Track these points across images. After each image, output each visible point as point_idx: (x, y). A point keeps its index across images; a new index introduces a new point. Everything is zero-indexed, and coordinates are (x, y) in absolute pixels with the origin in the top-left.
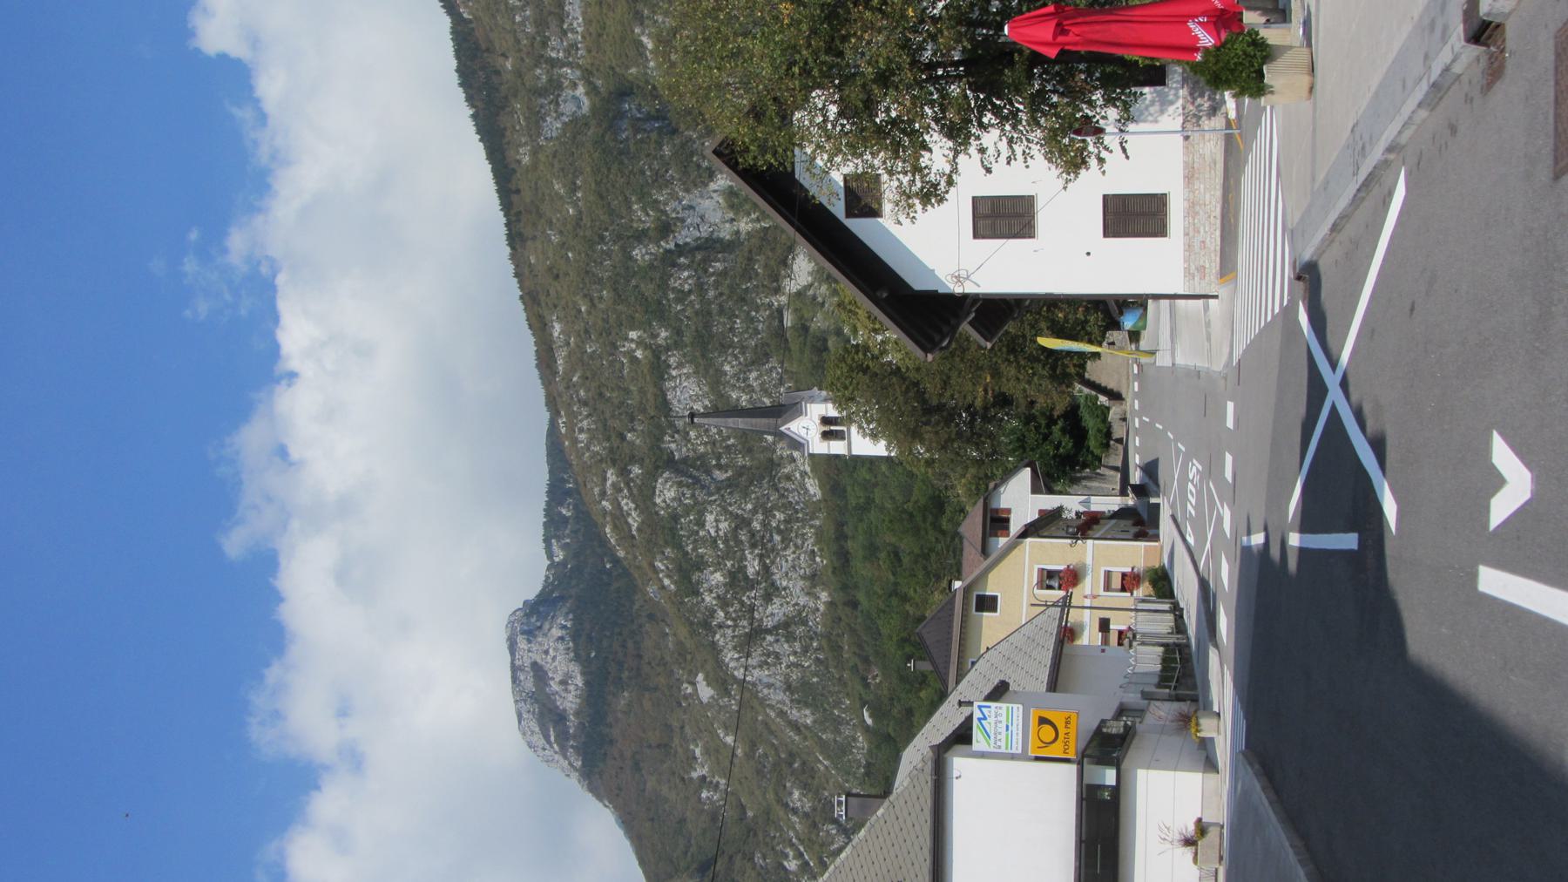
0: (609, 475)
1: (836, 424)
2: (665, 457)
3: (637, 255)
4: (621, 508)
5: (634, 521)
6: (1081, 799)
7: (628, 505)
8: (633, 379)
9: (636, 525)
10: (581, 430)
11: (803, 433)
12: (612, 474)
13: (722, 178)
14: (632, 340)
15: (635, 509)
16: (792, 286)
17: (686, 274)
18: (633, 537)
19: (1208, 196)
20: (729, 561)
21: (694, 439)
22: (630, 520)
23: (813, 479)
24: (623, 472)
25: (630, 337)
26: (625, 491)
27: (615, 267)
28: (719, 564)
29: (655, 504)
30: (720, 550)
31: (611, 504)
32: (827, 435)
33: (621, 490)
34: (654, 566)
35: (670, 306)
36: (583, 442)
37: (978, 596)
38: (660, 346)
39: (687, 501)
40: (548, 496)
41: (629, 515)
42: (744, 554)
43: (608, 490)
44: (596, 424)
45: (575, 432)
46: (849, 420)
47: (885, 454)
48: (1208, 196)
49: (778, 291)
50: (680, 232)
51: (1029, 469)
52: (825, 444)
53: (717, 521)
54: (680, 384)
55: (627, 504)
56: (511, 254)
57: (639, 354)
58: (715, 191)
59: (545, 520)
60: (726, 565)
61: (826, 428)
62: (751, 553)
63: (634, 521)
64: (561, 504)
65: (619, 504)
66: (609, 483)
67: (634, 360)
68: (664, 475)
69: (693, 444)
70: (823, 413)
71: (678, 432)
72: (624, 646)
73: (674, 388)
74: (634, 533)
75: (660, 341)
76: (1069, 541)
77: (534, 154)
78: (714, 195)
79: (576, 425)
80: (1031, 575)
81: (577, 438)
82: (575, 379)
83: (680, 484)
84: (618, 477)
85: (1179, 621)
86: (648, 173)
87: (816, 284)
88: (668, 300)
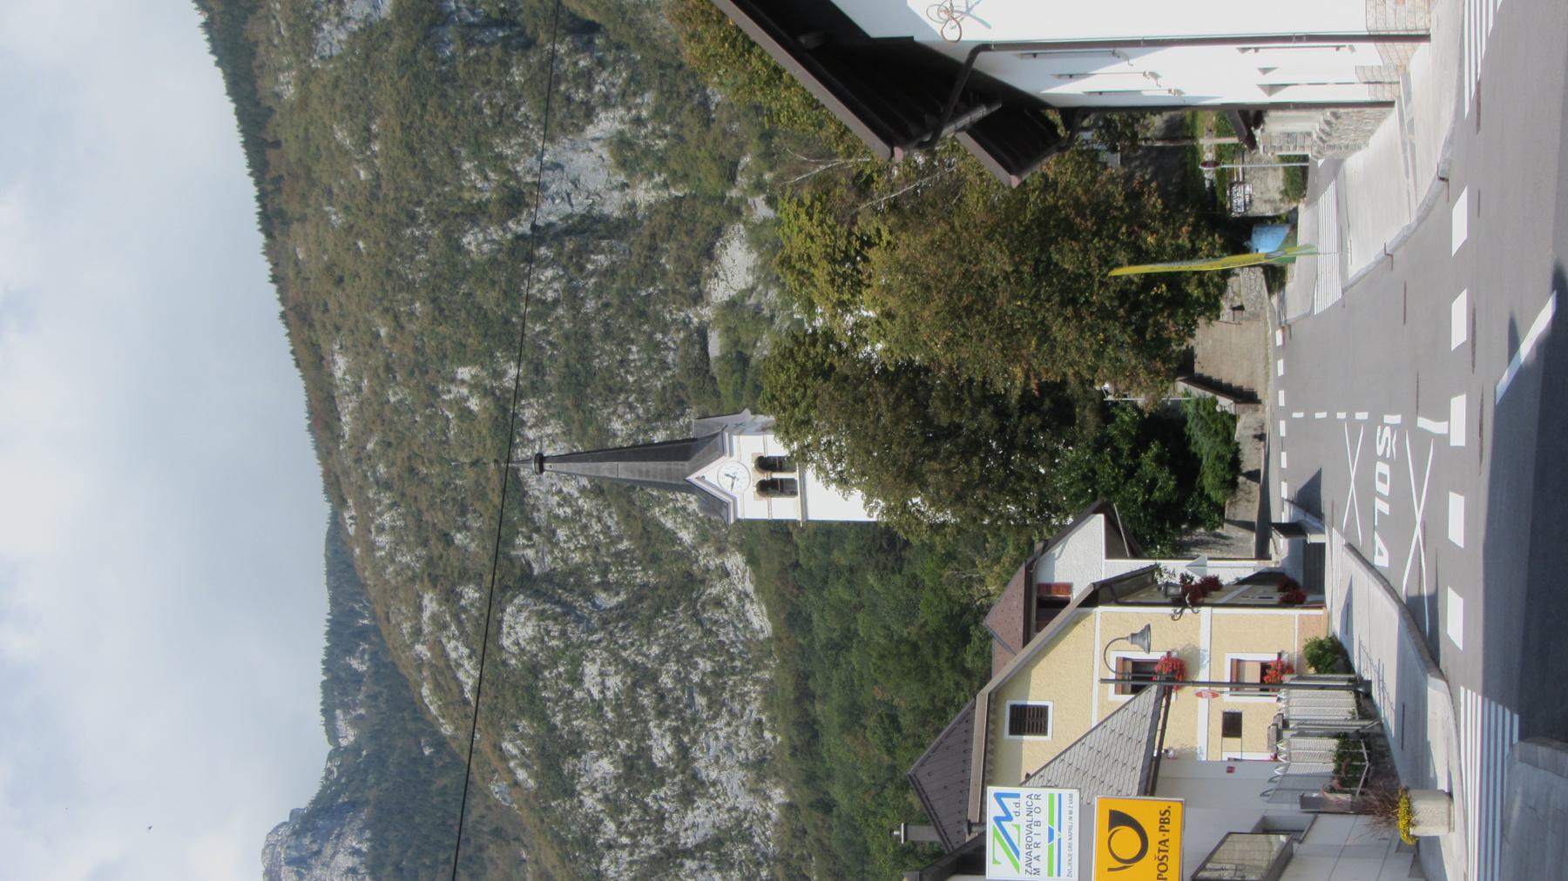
0: (426, 602)
1: (781, 470)
2: (518, 572)
5: (468, 676)
9: (471, 682)
10: (381, 529)
11: (725, 484)
13: (607, 119)
14: (463, 382)
15: (470, 657)
16: (719, 292)
17: (549, 273)
21: (565, 542)
22: (461, 675)
24: (450, 596)
25: (459, 377)
28: (606, 744)
29: (502, 648)
32: (766, 488)
37: (1014, 708)
40: (328, 640)
41: (460, 666)
49: (698, 298)
56: (266, 246)
57: (474, 404)
59: (325, 678)
61: (766, 476)
62: (659, 726)
64: (350, 652)
65: (443, 649)
66: (426, 615)
67: (465, 414)
68: (516, 601)
69: (562, 550)
70: (761, 451)
76: (1170, 610)
78: (594, 146)
83: (542, 615)
84: (440, 605)
87: (760, 287)
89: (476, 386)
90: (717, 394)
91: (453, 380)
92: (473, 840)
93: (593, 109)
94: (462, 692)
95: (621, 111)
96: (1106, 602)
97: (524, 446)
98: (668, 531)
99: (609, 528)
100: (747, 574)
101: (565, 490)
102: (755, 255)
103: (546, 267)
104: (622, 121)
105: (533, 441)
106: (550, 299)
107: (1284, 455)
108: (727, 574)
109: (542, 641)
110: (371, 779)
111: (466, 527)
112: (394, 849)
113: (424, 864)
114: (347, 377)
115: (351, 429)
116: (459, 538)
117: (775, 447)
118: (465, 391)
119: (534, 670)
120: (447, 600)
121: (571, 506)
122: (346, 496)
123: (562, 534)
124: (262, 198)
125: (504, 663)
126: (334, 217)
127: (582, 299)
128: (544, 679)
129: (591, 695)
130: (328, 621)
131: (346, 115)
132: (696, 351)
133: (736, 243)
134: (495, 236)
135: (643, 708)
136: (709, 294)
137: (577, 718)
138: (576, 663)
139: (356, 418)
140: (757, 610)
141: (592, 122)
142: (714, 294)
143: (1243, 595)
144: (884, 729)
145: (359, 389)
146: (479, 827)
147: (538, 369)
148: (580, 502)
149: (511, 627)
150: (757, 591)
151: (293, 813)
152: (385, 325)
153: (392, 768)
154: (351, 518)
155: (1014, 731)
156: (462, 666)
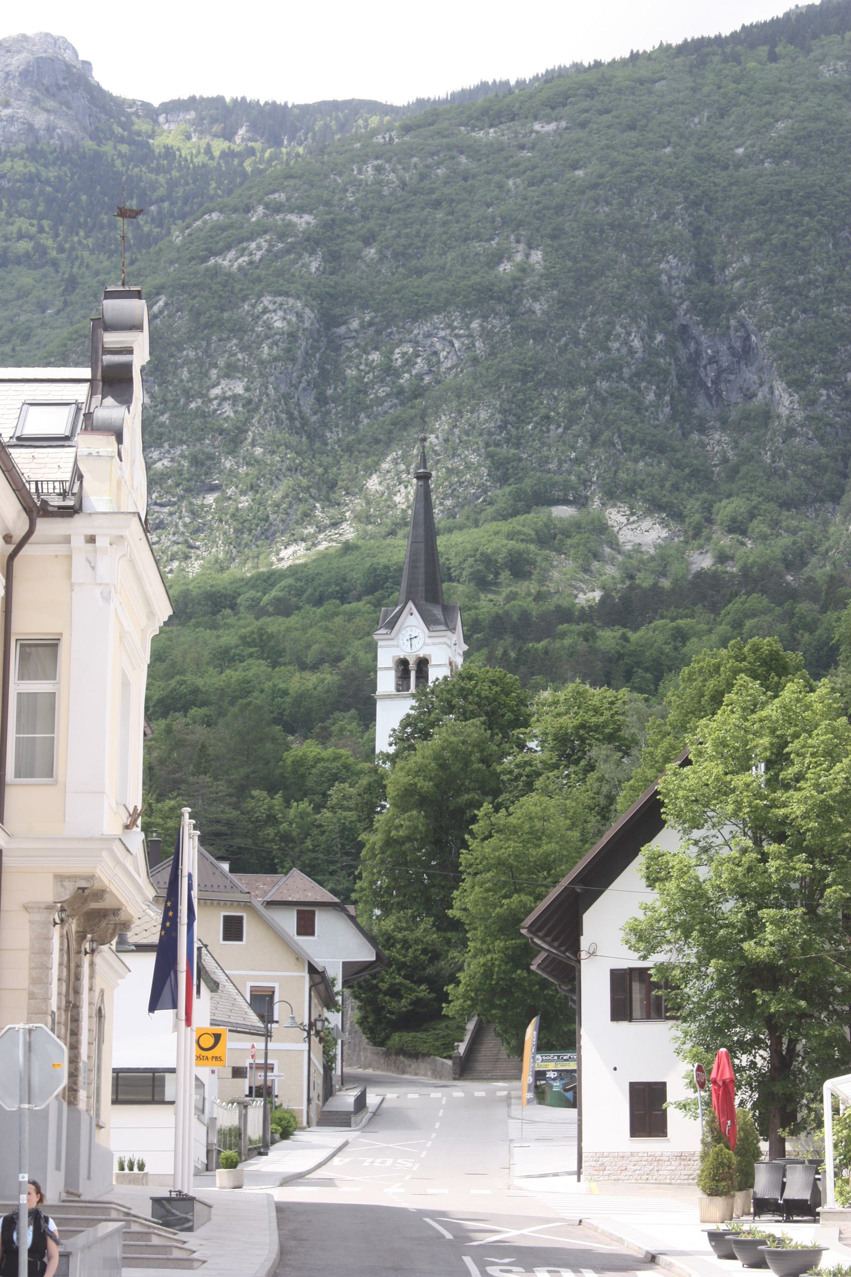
0: (307, 217)
1: (417, 678)
2: (337, 311)
3: (668, 262)
4: (251, 238)
5: (230, 262)
6: (154, 1071)
7: (258, 248)
8: (464, 258)
9: (226, 263)
10: (379, 169)
11: (405, 635)
12: (308, 223)
13: (791, 402)
14: (527, 256)
15: (251, 263)
16: (615, 516)
17: (637, 343)
18: (205, 259)
19: (666, 1173)
20: (169, 418)
21: (367, 359)
22: (232, 254)
23: (304, 555)
24: (311, 242)
25: (533, 252)
26: (280, 245)
27: (647, 226)
28: (165, 401)
29: (260, 296)
30: (187, 404)
31: (258, 223)
32: (403, 665)
33: (282, 236)
34: (158, 294)
35: (584, 318)
36: (360, 172)
37: (240, 919)
38: (519, 301)
39: (266, 350)
40: (266, 103)
41: (242, 252)
42: (182, 442)
43: (281, 216)
44: (391, 194)
45: (377, 158)
46: (421, 694)
47: (377, 751)
48: (666, 1173)
49: (611, 495)
50: (704, 332)
51: (374, 959)
52: (390, 664)
53: (235, 398)
54: (458, 336)
55: (259, 248)
56: (669, 46)
57: (506, 267)
58: (772, 392)
59: (228, 100)
60: (163, 414)
61: (412, 666)
62: (182, 456)
63: (230, 262)
64: (254, 127)
65: (259, 235)
66: (293, 218)
67: (499, 257)
68: (307, 310)
69: (359, 356)
70: (433, 662)
71: (378, 332)
72: (21, 236)
73: (450, 326)
74: (212, 261)
75: (527, 302)
76: (306, 1022)
77: (835, 86)
78: (766, 389)
79: (389, 161)
80: (266, 978)
81: (365, 162)
82: (463, 159)
83: (292, 336)
84: (304, 232)
85: (255, 1152)
86: (801, 278)
87: (620, 558)
88: (593, 315)
89: (524, 269)
90: (515, 513)
91: (530, 246)
92: (64, 256)
93: (803, 388)
94: (216, 254)
95: (800, 416)
96: (311, 979)
97: (463, 319)
98: (377, 463)
99: (382, 405)
100: (334, 544)
101: (419, 360)
102: (652, 551)
103: (642, 339)
104: (790, 417)
105: (468, 328)
106: (610, 344)
107: (417, 1096)
108: (335, 525)
109: (267, 337)
110: (124, 148)
111: (382, 258)
112: (52, 173)
113: (38, 205)
114: (534, 135)
115: (481, 139)
116: (371, 252)
117: (436, 673)
118: (519, 258)
119: (238, 329)
120: (308, 239)
121: (403, 366)
122: (412, 133)
123: (375, 356)
124: (718, 40)
125: (244, 299)
126: (696, 120)
127: (610, 376)
128: (228, 339)
129: (214, 387)
130: (286, 103)
131: (802, 133)
132: (557, 494)
133: (664, 533)
134: (675, 287)
135: (201, 439)
136: (614, 506)
137: (190, 372)
138: (246, 371)
139: (492, 145)
140: (299, 553)
141: (789, 387)
142: (614, 511)
143: (316, 1070)
144: (185, 695)
145: (522, 147)
146: (77, 263)
147: (539, 335)
148: (407, 375)
149: (281, 304)
150: (319, 553)
151: (87, 64)
152: (586, 174)
153: (137, 170)
154: (391, 139)
155: (227, 919)
156: (242, 255)
